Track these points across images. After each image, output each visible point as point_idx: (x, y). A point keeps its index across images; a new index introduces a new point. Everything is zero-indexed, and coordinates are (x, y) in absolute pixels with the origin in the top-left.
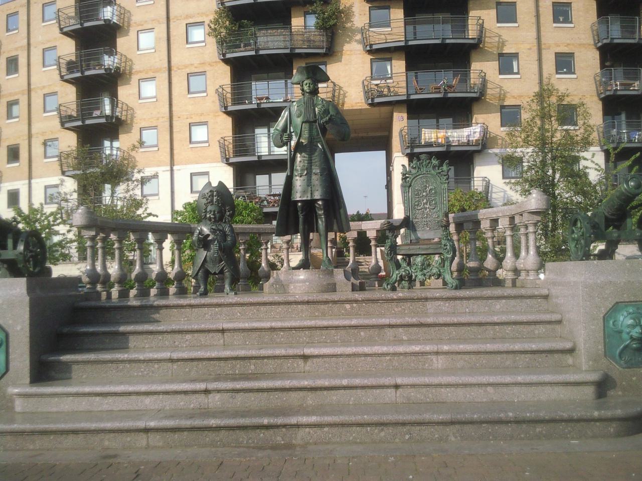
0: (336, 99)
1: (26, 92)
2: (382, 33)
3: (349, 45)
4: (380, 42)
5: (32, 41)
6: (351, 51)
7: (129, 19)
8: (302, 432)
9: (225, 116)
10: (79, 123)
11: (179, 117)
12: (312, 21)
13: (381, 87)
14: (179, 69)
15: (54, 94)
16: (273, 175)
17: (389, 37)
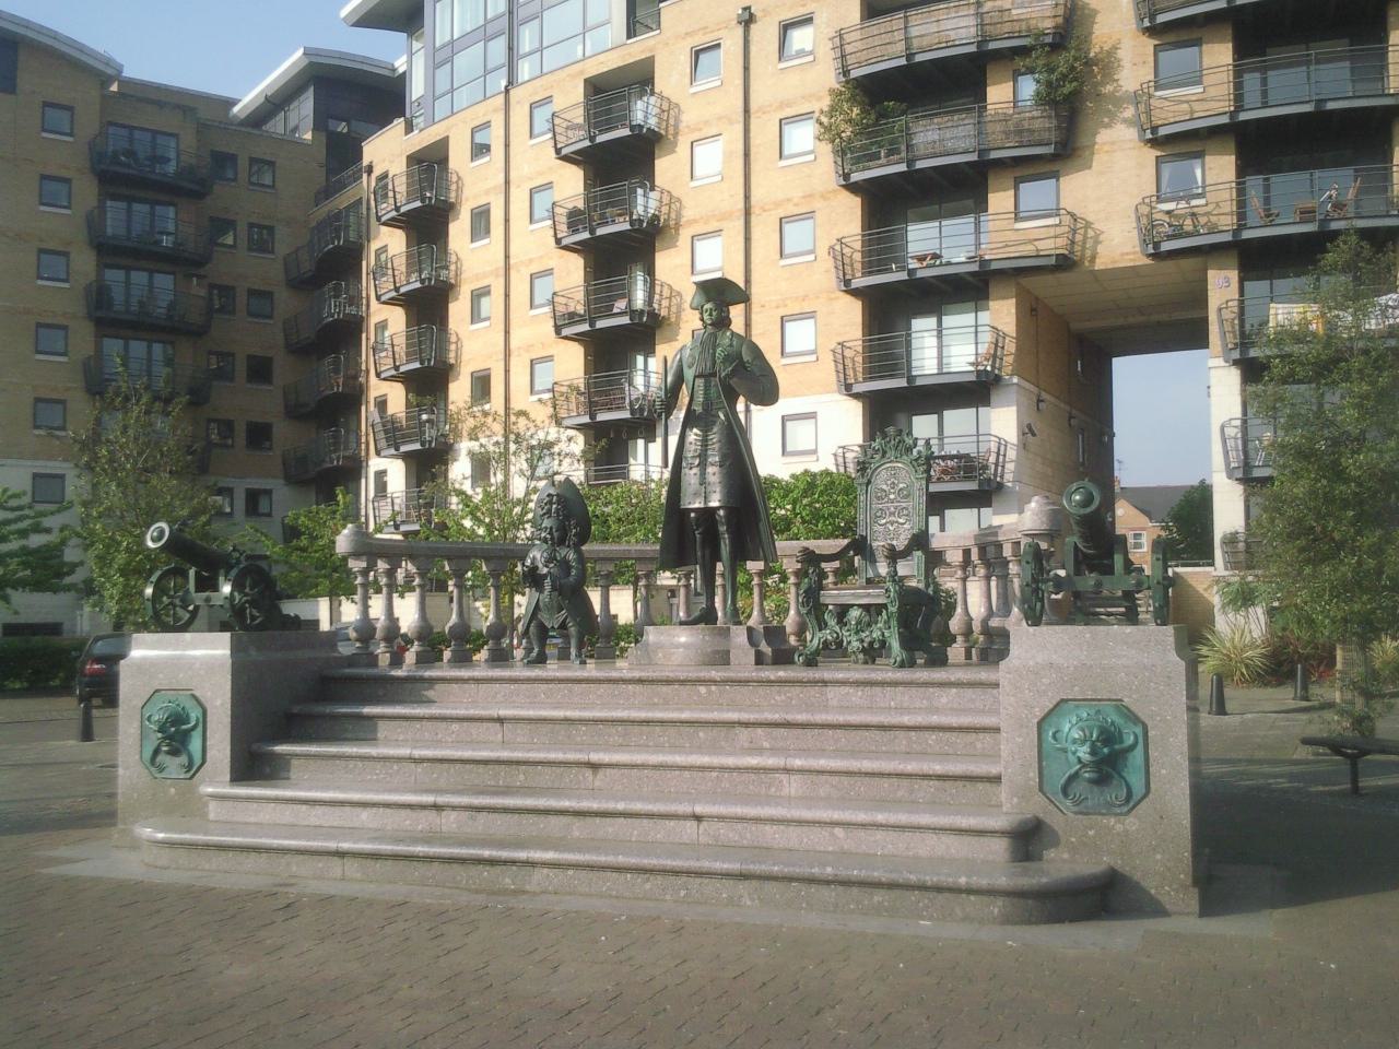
0: (1077, 248)
1: (502, 272)
2: (1183, 99)
3: (1108, 131)
4: (1177, 119)
5: (513, 175)
6: (1113, 143)
7: (677, 120)
8: (539, 875)
9: (848, 298)
10: (585, 327)
11: (763, 306)
12: (1028, 87)
13: (1178, 217)
14: (765, 211)
15: (549, 272)
16: (948, 414)
17: (1196, 106)
